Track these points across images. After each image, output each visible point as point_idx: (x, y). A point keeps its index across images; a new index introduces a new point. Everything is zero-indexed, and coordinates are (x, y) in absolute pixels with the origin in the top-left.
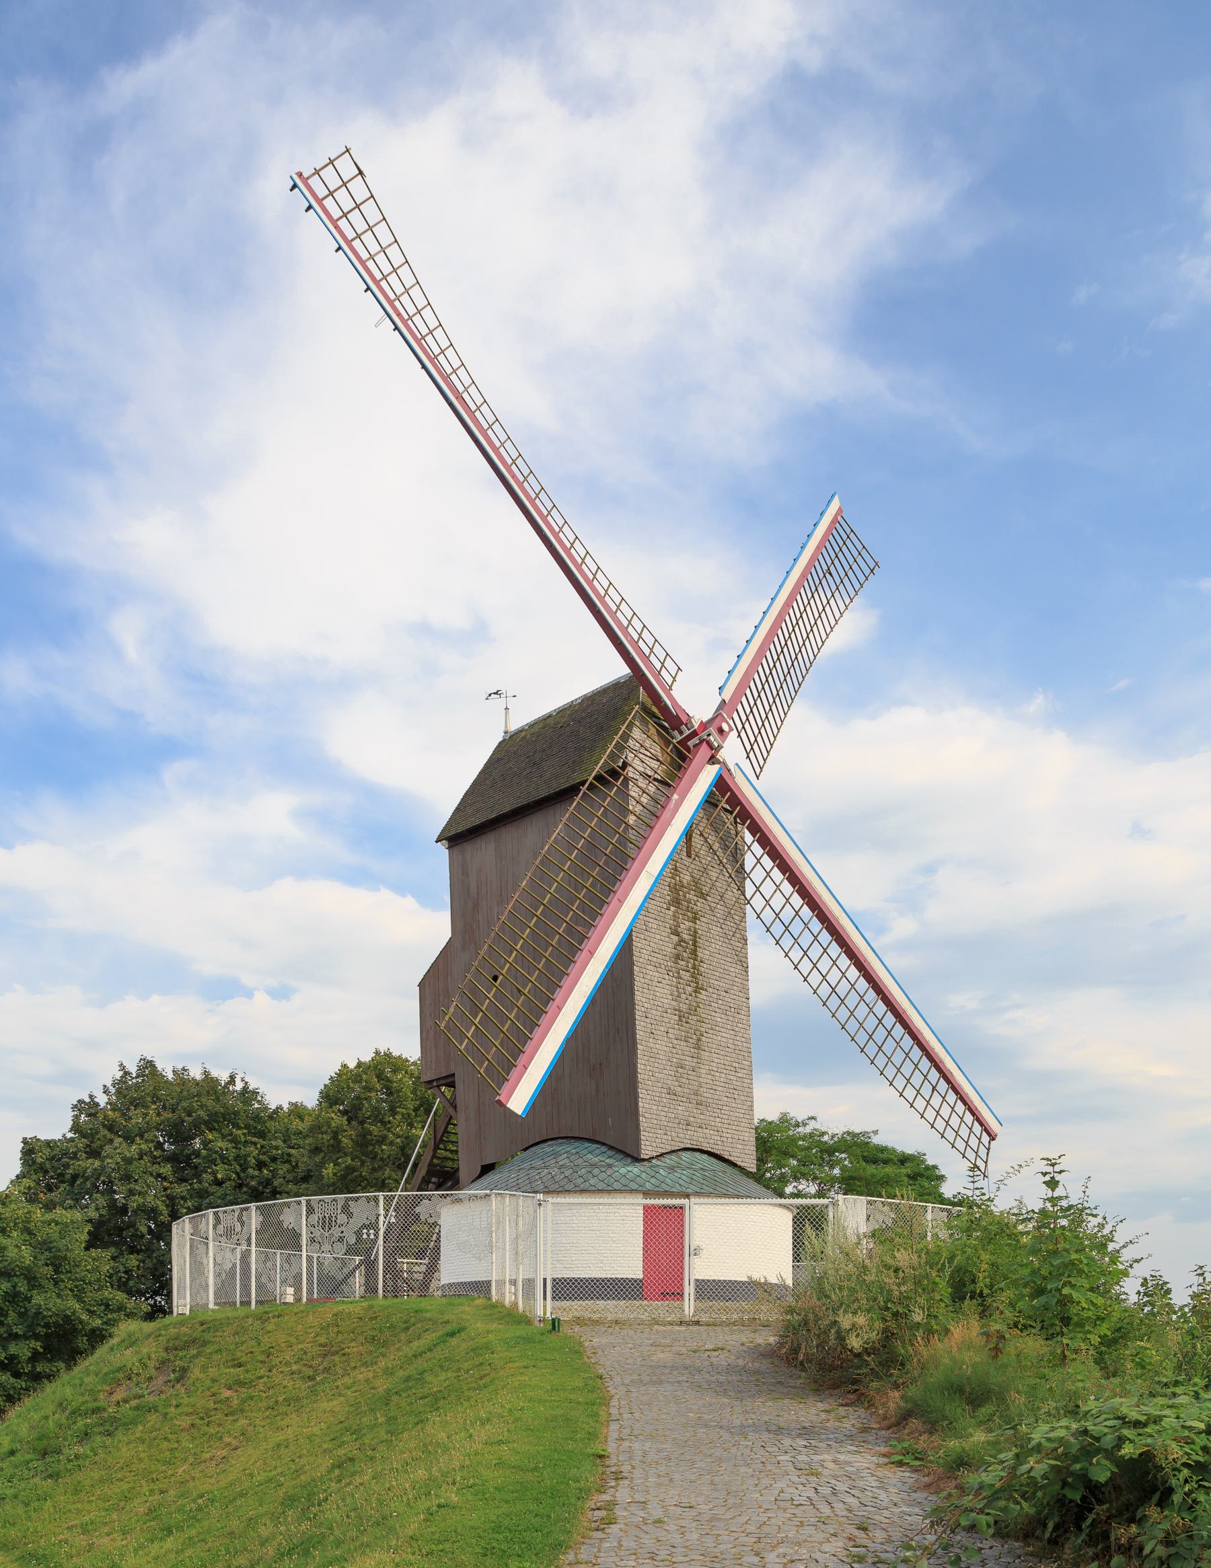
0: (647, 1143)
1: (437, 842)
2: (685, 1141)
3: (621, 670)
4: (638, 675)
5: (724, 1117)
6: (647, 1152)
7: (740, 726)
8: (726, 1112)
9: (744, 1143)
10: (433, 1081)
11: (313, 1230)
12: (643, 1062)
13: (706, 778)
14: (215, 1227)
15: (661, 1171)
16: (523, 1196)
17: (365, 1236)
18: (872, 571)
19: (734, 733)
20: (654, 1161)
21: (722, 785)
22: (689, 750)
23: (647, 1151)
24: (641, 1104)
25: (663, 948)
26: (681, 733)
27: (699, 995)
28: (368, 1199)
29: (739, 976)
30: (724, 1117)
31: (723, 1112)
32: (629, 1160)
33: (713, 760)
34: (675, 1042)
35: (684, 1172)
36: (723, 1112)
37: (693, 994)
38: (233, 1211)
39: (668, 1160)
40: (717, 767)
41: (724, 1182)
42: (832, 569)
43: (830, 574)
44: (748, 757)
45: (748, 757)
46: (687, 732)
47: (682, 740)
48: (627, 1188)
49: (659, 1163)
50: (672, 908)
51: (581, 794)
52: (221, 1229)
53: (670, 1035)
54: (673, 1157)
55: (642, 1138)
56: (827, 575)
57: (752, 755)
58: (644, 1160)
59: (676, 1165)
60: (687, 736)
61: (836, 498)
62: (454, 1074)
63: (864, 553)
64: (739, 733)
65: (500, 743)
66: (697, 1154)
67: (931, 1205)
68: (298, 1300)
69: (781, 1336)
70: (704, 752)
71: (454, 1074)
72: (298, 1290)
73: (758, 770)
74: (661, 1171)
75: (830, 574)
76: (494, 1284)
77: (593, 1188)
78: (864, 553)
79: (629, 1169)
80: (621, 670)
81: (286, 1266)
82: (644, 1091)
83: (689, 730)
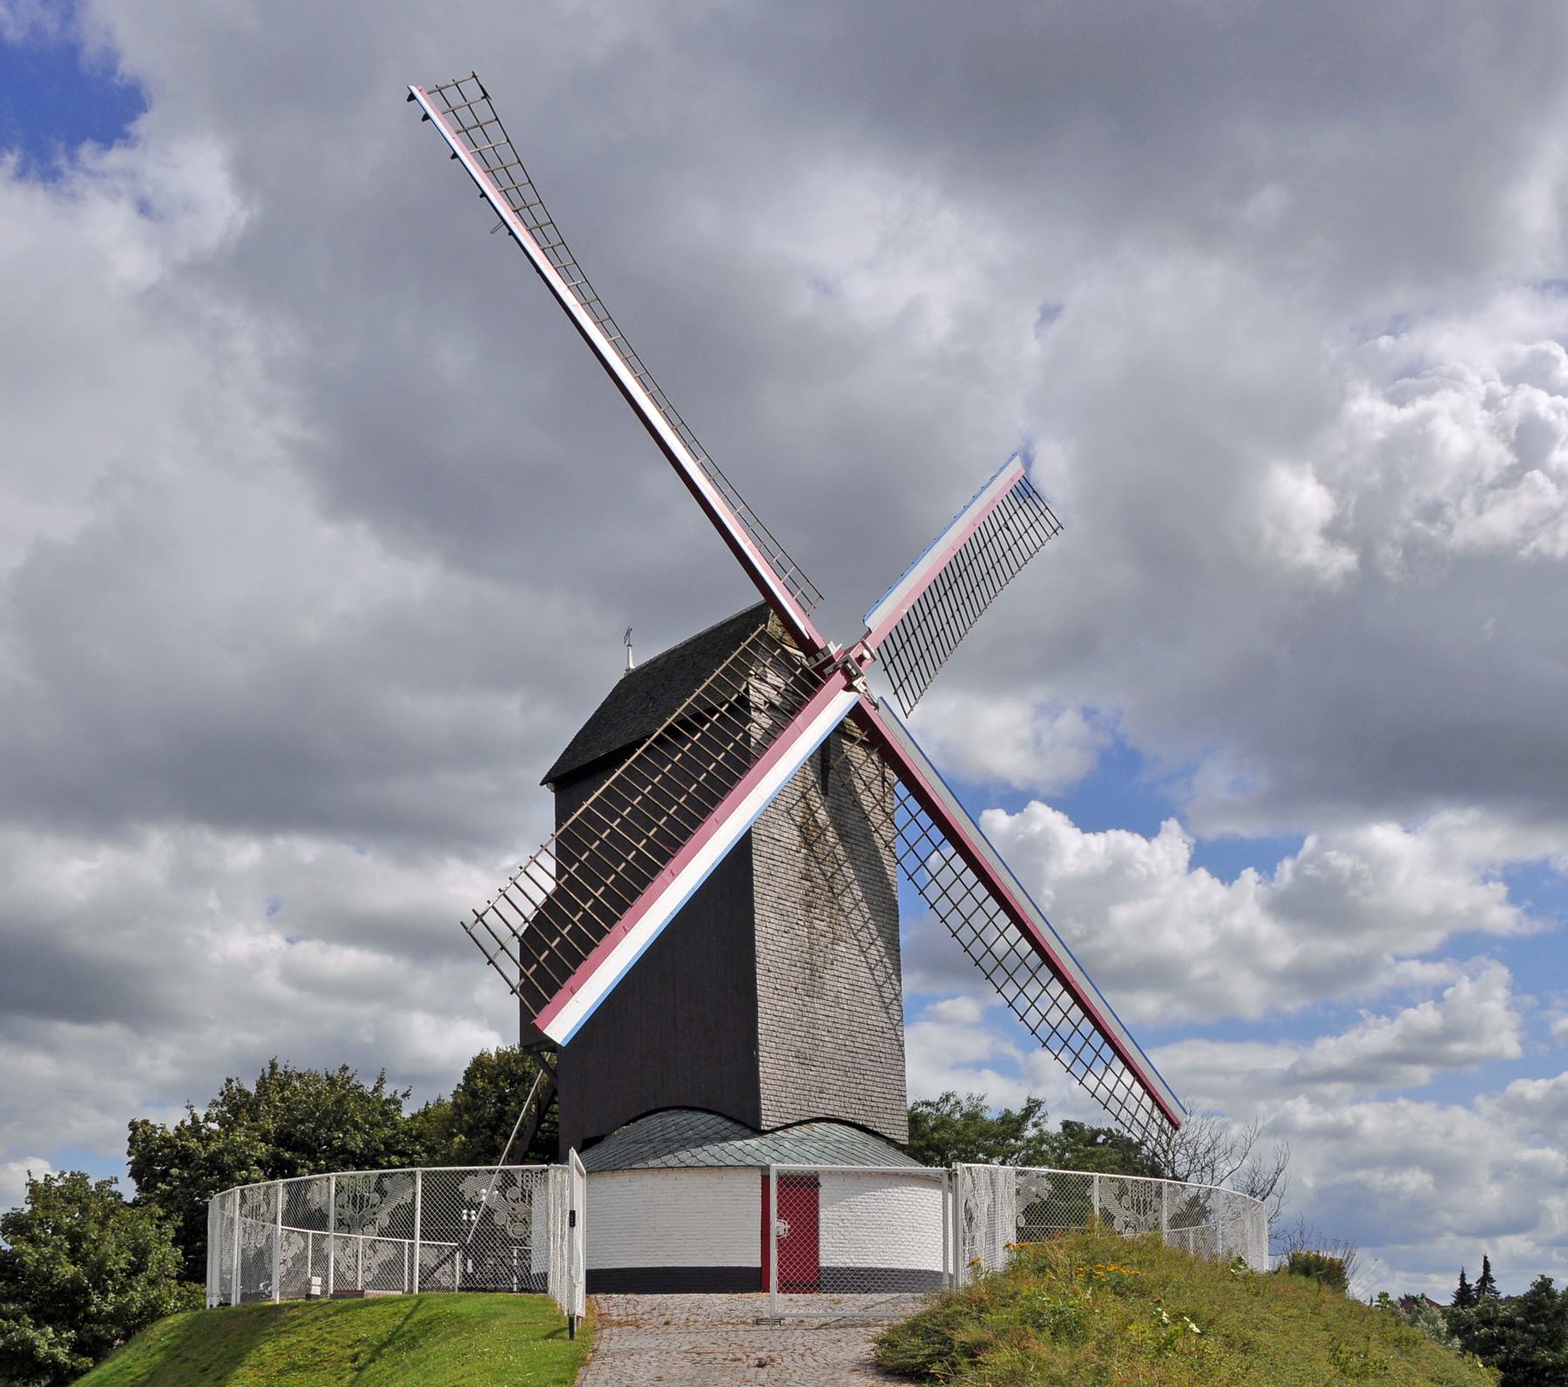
0: (769, 1113)
1: (541, 784)
2: (819, 1110)
5: (868, 1083)
6: (768, 1123)
8: (870, 1078)
9: (892, 1112)
11: (341, 1210)
12: (765, 1021)
15: (787, 1144)
17: (465, 1218)
18: (1055, 531)
20: (778, 1133)
22: (823, 676)
23: (765, 1124)
24: (761, 1069)
25: (791, 894)
26: (817, 660)
27: (837, 947)
29: (887, 926)
30: (868, 1083)
31: (866, 1077)
32: (748, 1132)
34: (807, 999)
35: (814, 1145)
36: (866, 1077)
37: (830, 946)
39: (796, 1132)
40: (853, 695)
41: (862, 1156)
42: (1010, 523)
43: (1008, 528)
46: (822, 659)
47: (817, 666)
48: (742, 1164)
50: (803, 851)
52: (246, 1207)
53: (799, 991)
54: (804, 1128)
55: (763, 1107)
57: (900, 691)
59: (806, 1137)
60: (821, 664)
65: (621, 681)
66: (835, 1126)
67: (1099, 1174)
68: (324, 1292)
69: (881, 1342)
70: (839, 679)
72: (325, 1282)
74: (787, 1144)
75: (1008, 528)
77: (702, 1164)
80: (758, 598)
81: (370, 1252)
83: (825, 656)
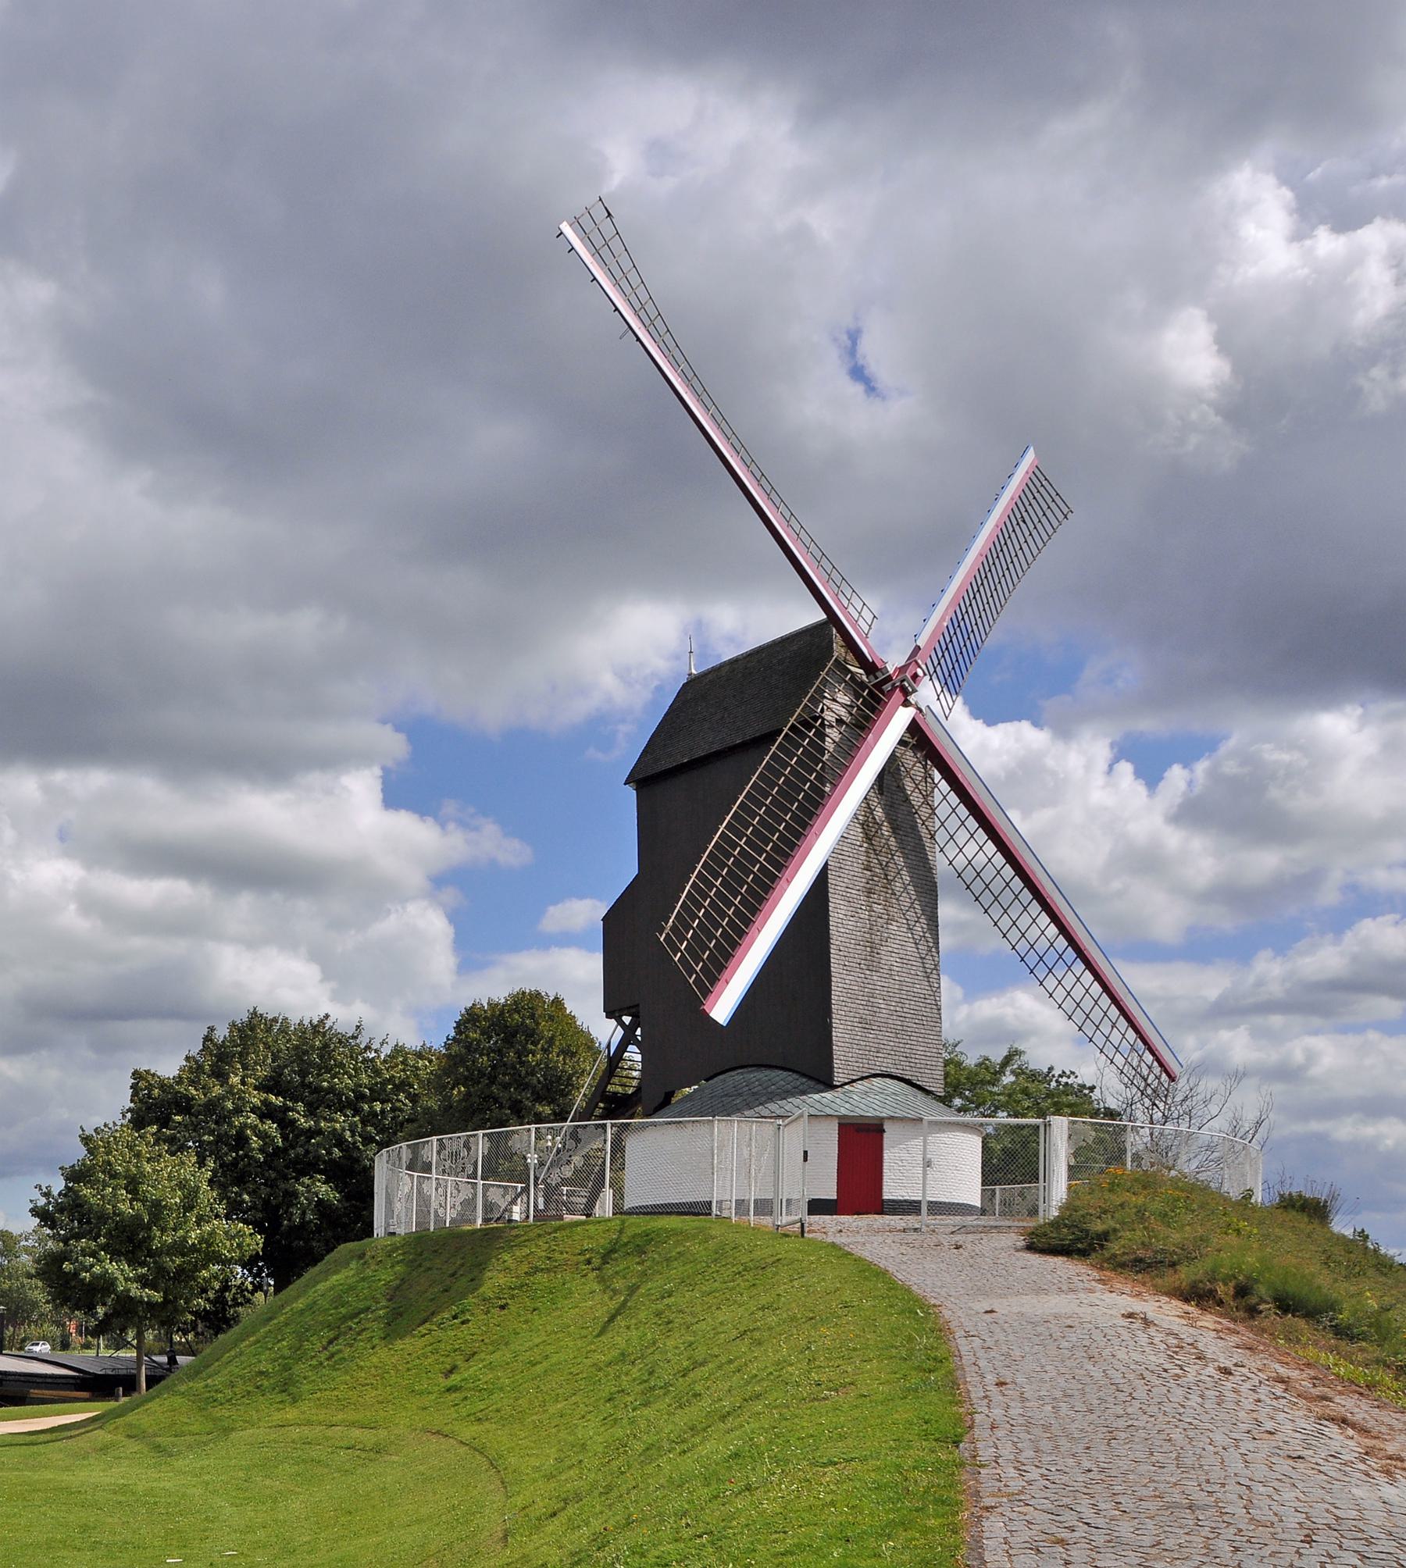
0: (840, 1070)
1: (625, 784)
3: (822, 616)
4: (832, 618)
7: (932, 670)
10: (614, 1011)
13: (899, 720)
14: (439, 1153)
16: (756, 1122)
19: (928, 677)
20: (846, 1087)
21: (914, 728)
22: (882, 692)
25: (856, 883)
28: (597, 1126)
33: (906, 704)
38: (459, 1137)
39: (859, 1085)
43: (1024, 521)
44: (938, 699)
45: (938, 699)
49: (851, 1089)
51: (783, 735)
56: (1021, 523)
57: (942, 696)
58: (838, 1087)
61: (1032, 449)
62: (638, 1005)
63: (1057, 499)
64: (931, 676)
71: (638, 1005)
73: (947, 712)
75: (1024, 521)
76: (714, 1204)
78: (1057, 499)
79: (823, 1095)
80: (822, 616)
82: (838, 1021)
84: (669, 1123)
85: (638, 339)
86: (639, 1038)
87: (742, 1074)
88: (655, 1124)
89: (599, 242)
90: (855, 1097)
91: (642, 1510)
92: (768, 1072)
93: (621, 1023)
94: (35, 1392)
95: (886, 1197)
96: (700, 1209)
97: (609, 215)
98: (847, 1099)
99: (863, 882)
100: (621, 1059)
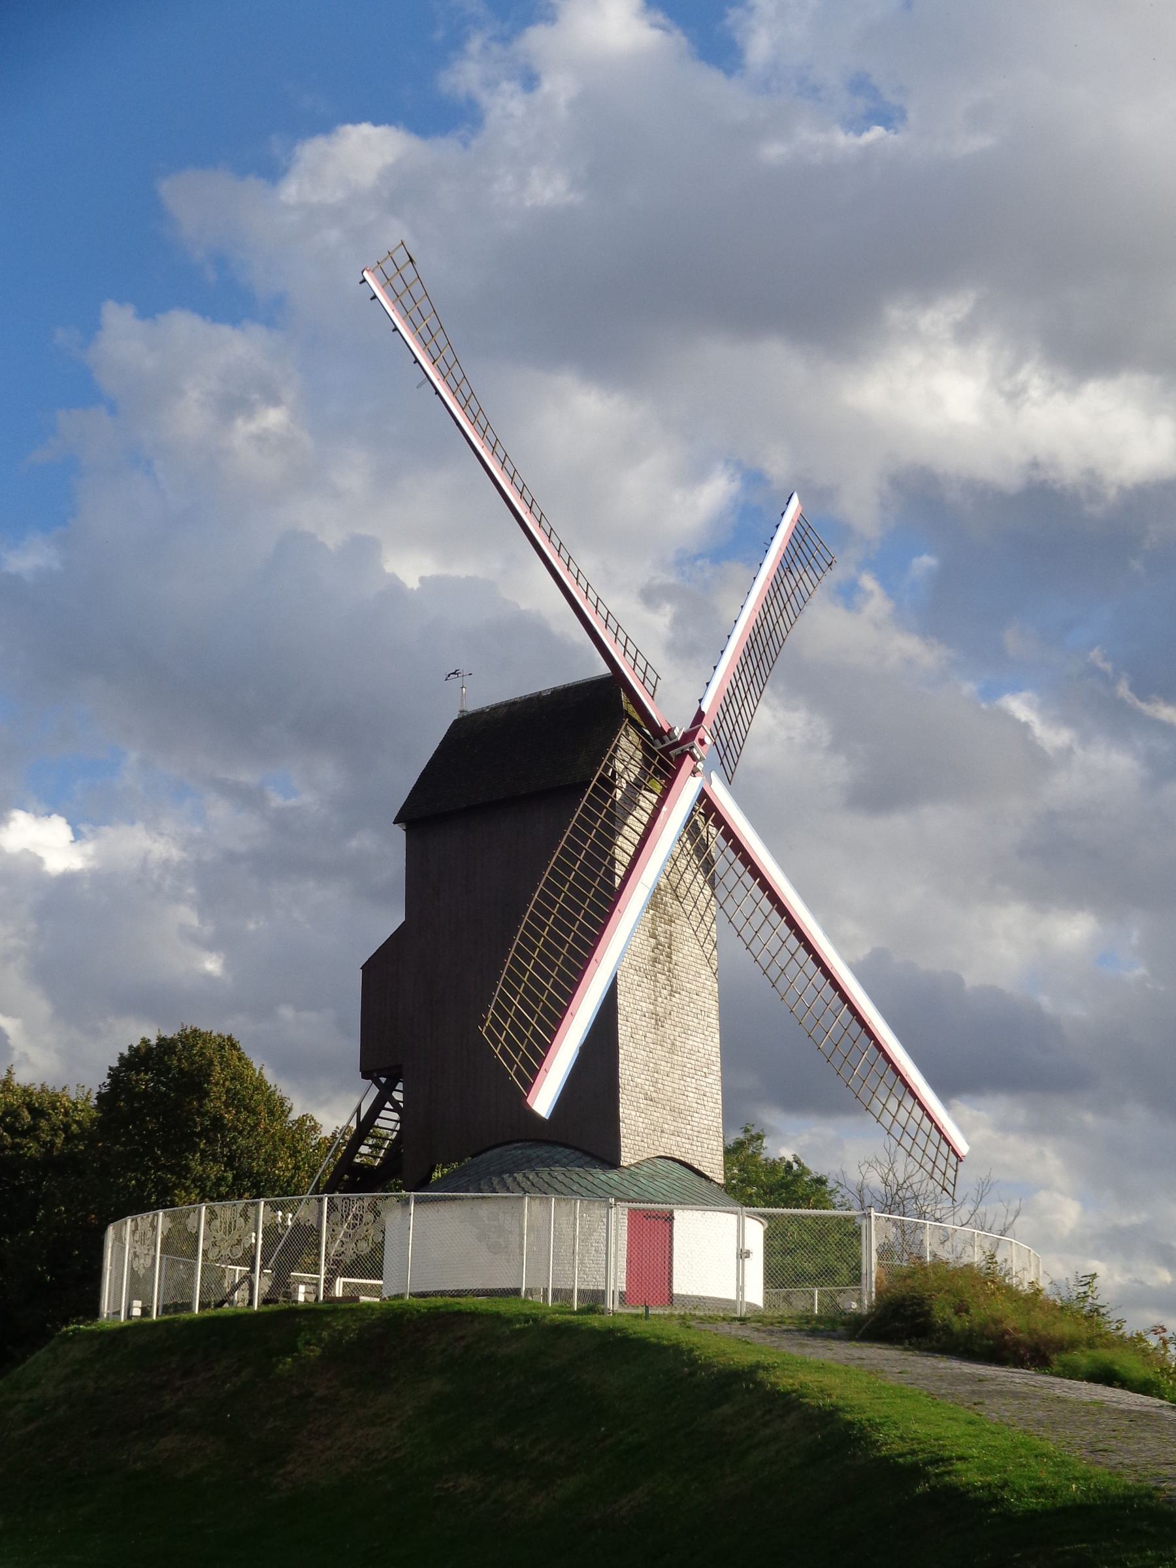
1: (394, 823)
22: (670, 758)
43: (790, 571)
56: (788, 573)
84: (478, 1198)
85: (437, 392)
86: (402, 1105)
87: (520, 1148)
88: (461, 1198)
89: (399, 286)
90: (642, 1179)
91: (986, 1283)
92: (547, 1148)
93: (377, 1082)
94: (740, 1284)
95: (676, 1290)
96: (517, 1292)
97: (411, 260)
98: (634, 1182)
99: (648, 953)
100: (372, 1125)
